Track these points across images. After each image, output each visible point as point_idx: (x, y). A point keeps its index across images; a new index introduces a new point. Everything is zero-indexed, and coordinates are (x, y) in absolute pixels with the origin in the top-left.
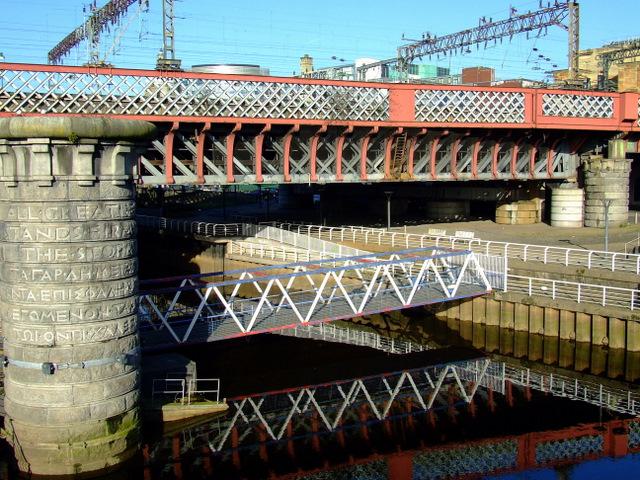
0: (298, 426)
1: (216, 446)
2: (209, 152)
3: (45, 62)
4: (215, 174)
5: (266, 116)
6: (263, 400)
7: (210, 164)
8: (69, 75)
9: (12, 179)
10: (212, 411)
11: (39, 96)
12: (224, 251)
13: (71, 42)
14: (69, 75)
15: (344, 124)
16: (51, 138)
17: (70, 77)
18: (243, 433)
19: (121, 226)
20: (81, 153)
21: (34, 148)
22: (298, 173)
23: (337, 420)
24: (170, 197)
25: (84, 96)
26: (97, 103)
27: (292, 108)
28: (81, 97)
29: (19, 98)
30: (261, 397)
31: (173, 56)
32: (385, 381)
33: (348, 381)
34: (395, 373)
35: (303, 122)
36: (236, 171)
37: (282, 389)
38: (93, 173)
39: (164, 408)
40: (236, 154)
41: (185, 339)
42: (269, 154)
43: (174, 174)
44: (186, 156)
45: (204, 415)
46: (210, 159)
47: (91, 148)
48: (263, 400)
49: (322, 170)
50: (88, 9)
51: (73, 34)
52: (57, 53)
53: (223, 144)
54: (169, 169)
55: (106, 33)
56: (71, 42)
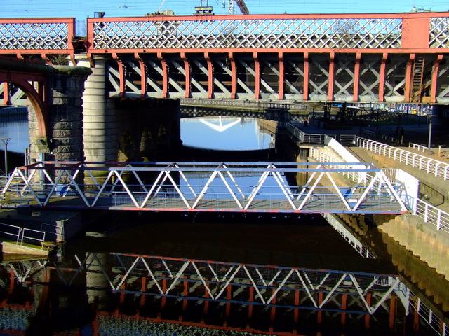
0: (352, 303)
1: (116, 286)
2: (242, 75)
4: (222, 92)
5: (312, 46)
6: (279, 272)
8: (372, 20)
10: (36, 253)
11: (382, 36)
12: (308, 155)
14: (372, 20)
15: (353, 51)
17: (373, 21)
18: (73, 272)
22: (319, 93)
23: (271, 299)
24: (361, 116)
25: (305, 35)
26: (271, 40)
28: (379, 36)
29: (357, 38)
30: (327, 273)
32: (257, 270)
33: (337, 272)
34: (182, 260)
35: (390, 51)
37: (206, 260)
41: (93, 205)
42: (292, 77)
44: (201, 78)
45: (30, 255)
46: (243, 81)
48: (279, 272)
49: (340, 92)
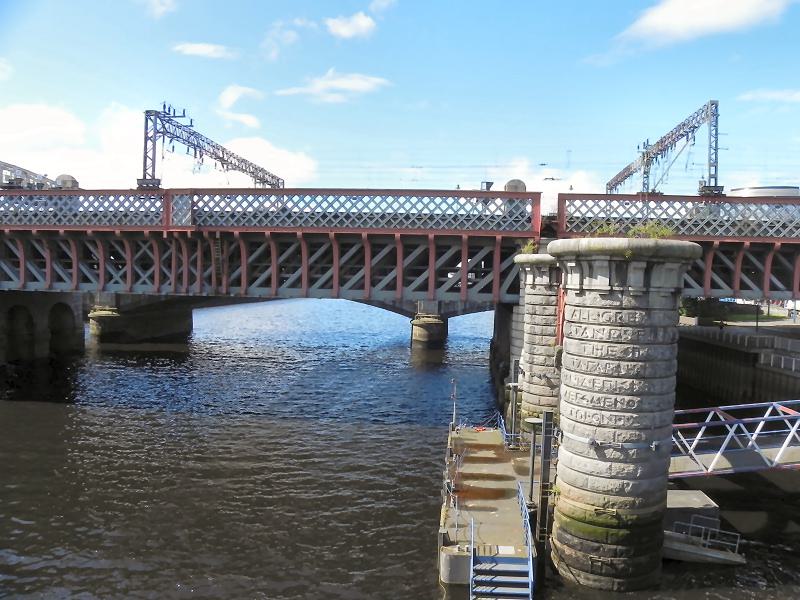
3: (604, 192)
7: (199, 263)
9: (578, 287)
13: (627, 173)
16: (611, 256)
19: (665, 332)
20: (635, 268)
21: (597, 264)
27: (65, 217)
31: (716, 183)
36: (714, 285)
38: (645, 286)
39: (672, 458)
40: (774, 272)
43: (741, 288)
47: (644, 265)
50: (641, 147)
51: (628, 169)
52: (612, 185)
53: (789, 261)
54: (708, 283)
55: (656, 165)
56: (627, 173)
